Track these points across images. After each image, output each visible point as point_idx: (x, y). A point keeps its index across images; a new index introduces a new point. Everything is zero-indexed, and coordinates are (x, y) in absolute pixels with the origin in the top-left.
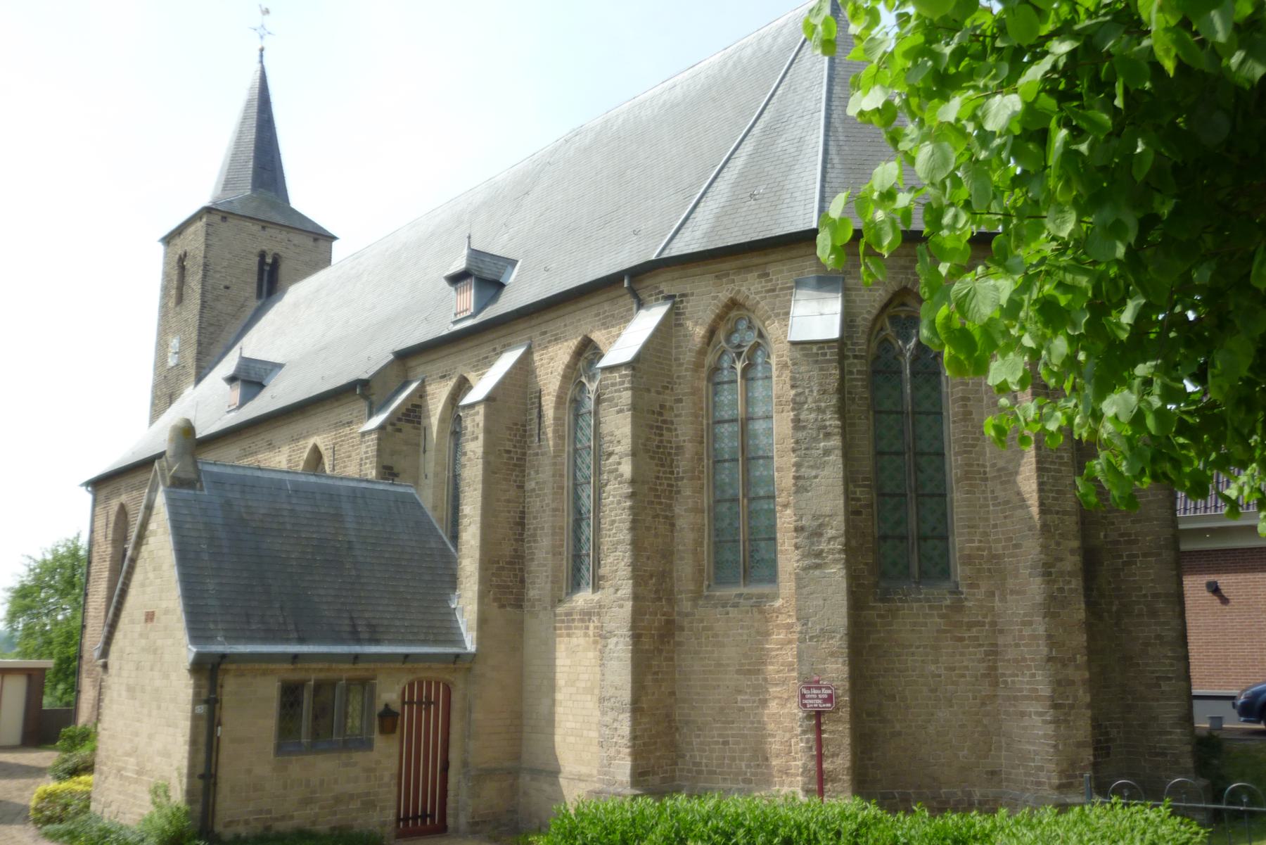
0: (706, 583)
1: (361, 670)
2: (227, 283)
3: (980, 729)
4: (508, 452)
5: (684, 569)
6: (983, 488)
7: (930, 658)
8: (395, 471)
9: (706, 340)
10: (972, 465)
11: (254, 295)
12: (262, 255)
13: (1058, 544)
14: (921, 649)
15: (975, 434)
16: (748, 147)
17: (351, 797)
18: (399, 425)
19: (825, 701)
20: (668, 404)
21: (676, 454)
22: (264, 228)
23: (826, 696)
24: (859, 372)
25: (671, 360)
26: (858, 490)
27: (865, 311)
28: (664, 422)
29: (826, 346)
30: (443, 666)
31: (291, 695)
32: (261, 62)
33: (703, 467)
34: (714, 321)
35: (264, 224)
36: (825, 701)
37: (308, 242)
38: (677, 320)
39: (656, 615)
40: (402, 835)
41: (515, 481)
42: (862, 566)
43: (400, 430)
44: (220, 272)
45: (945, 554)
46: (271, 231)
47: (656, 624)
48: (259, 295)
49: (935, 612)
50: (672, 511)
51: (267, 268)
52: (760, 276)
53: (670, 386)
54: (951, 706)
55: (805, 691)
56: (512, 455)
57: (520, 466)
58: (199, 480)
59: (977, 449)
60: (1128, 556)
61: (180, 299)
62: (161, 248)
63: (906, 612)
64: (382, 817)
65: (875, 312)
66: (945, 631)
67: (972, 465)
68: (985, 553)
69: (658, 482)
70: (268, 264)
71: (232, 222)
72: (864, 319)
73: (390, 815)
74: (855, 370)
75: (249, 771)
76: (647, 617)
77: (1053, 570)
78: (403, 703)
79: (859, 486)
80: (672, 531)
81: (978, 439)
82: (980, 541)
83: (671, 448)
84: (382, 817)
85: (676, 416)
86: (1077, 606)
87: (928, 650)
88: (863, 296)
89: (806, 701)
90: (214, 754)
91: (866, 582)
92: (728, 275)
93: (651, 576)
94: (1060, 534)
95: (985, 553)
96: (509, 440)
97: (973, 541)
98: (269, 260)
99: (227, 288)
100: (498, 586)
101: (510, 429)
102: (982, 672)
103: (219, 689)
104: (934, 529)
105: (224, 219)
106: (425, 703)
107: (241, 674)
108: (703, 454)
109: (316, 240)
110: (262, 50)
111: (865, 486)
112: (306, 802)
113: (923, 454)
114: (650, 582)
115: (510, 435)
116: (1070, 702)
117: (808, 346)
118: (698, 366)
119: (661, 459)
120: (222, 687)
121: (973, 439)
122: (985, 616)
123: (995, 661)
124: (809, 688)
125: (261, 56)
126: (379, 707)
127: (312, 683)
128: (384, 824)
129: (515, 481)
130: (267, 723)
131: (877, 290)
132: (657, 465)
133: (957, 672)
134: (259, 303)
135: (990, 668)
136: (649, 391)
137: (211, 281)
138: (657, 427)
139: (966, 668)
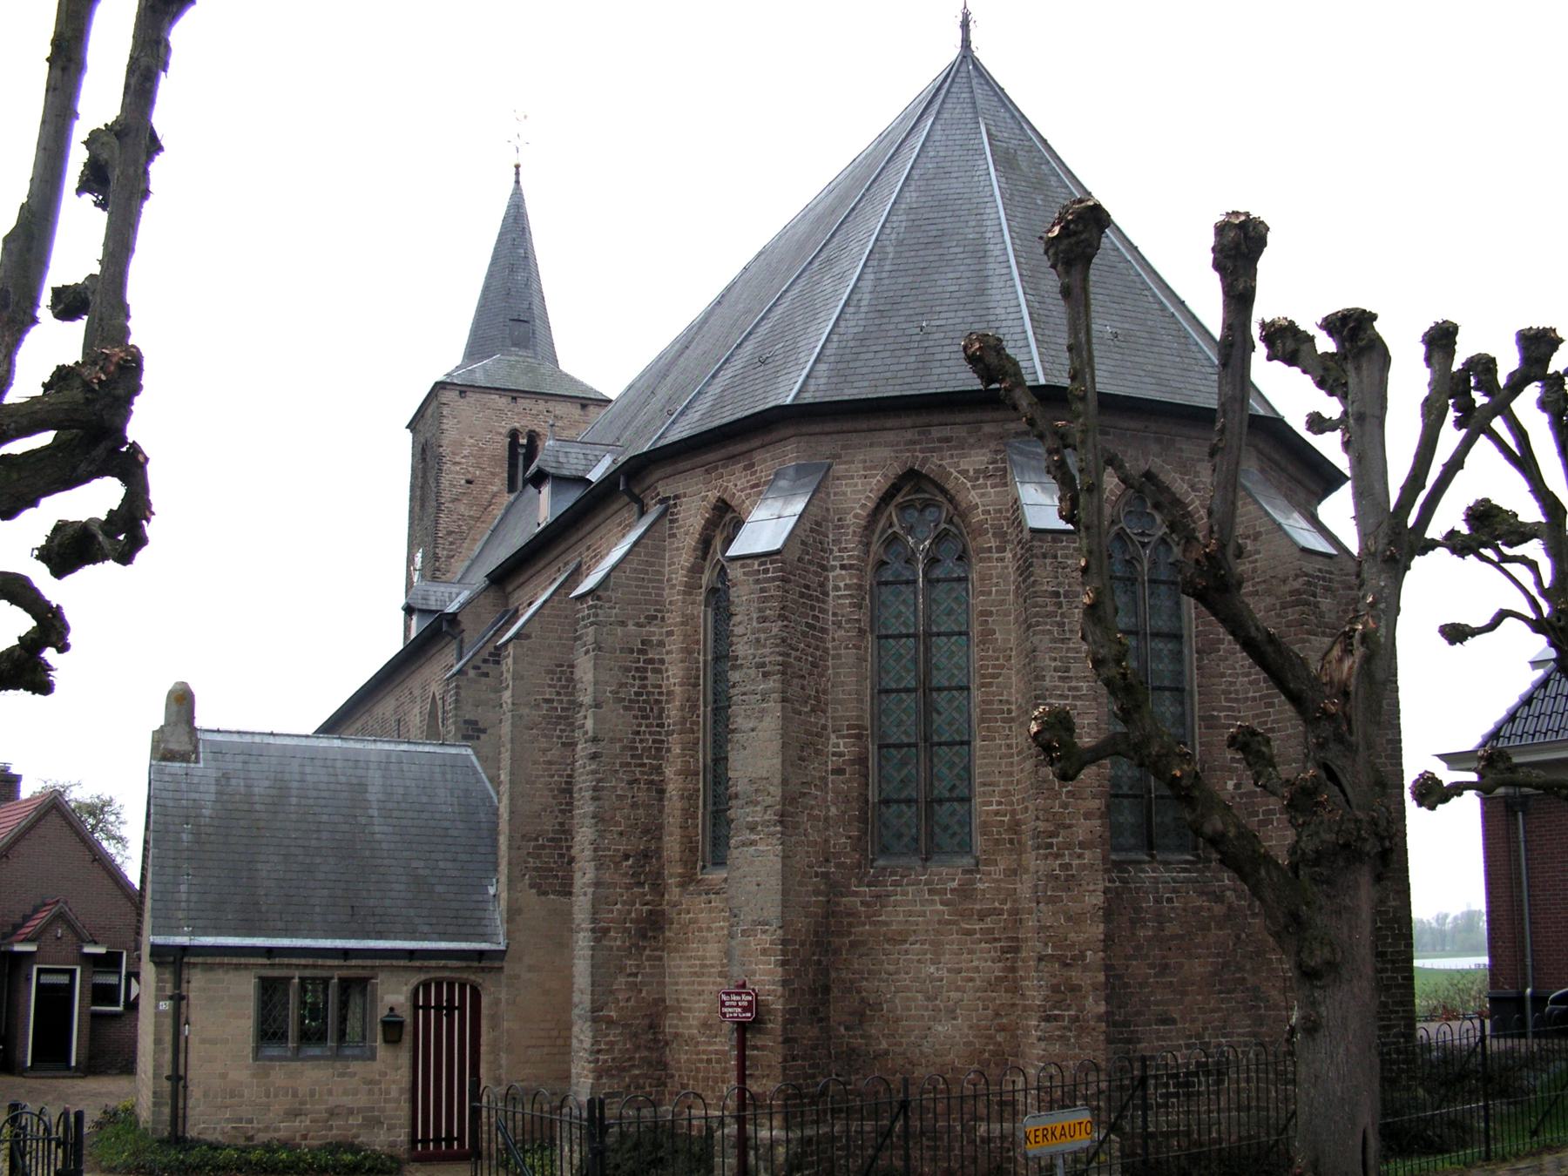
0: (700, 864)
1: (354, 969)
2: (469, 477)
3: (991, 1047)
4: (547, 701)
5: (672, 845)
6: (1007, 732)
7: (929, 956)
8: (481, 725)
9: (699, 553)
10: (991, 702)
11: (506, 488)
12: (514, 435)
13: (1065, 806)
14: (917, 946)
15: (997, 659)
16: (797, 289)
17: (351, 1112)
18: (485, 668)
19: (745, 1009)
20: (655, 639)
21: (668, 702)
22: (514, 399)
23: (746, 1004)
24: (847, 587)
25: (661, 581)
26: (841, 742)
27: (857, 506)
28: (651, 661)
29: (768, 559)
30: (464, 964)
31: (270, 990)
32: (517, 182)
33: (698, 716)
34: (705, 528)
35: (514, 395)
36: (745, 1009)
37: (575, 411)
38: (671, 528)
39: (634, 904)
40: (424, 1159)
41: (560, 737)
42: (843, 840)
43: (486, 675)
44: (459, 463)
45: (966, 822)
46: (523, 403)
47: (633, 915)
48: (512, 487)
49: (937, 898)
50: (662, 773)
51: (522, 451)
52: (746, 468)
53: (659, 615)
54: (954, 1019)
55: (724, 997)
56: (555, 704)
57: (567, 718)
58: (196, 750)
59: (1000, 679)
60: (1265, 813)
61: (422, 506)
62: (408, 435)
63: (899, 897)
64: (390, 1136)
65: (871, 505)
66: (949, 922)
67: (991, 702)
68: (1006, 819)
69: (637, 738)
70: (523, 446)
71: (472, 397)
72: (856, 516)
73: (402, 1136)
74: (842, 585)
75: (224, 1076)
76: (619, 906)
77: (1054, 840)
78: (416, 1007)
79: (843, 737)
80: (661, 800)
81: (1002, 667)
82: (999, 803)
83: (660, 694)
84: (390, 1136)
85: (668, 653)
86: (1091, 887)
87: (926, 947)
88: (856, 485)
89: (725, 1010)
90: (182, 1056)
91: (848, 861)
92: (716, 468)
93: (627, 857)
94: (1069, 792)
95: (1006, 819)
96: (550, 686)
97: (990, 803)
98: (523, 441)
99: (469, 482)
100: (536, 869)
101: (548, 672)
102: (997, 974)
103: (184, 985)
104: (953, 787)
105: (462, 393)
106: (446, 1008)
107: (209, 967)
108: (698, 699)
109: (584, 407)
110: (517, 167)
111: (849, 736)
112: (295, 1114)
113: (888, 691)
114: (625, 863)
115: (552, 679)
116: (1072, 1013)
117: (749, 561)
118: (690, 588)
119: (640, 709)
120: (188, 982)
121: (994, 667)
122: (1004, 902)
123: (1015, 960)
124: (728, 994)
125: (517, 174)
126: (382, 1012)
127: (336, 980)
128: (393, 1145)
129: (560, 737)
130: (245, 1024)
131: (874, 476)
132: (636, 717)
133: (964, 974)
134: (512, 497)
135: (1005, 969)
136: (623, 624)
137: (448, 477)
138: (637, 669)
139: (977, 969)
